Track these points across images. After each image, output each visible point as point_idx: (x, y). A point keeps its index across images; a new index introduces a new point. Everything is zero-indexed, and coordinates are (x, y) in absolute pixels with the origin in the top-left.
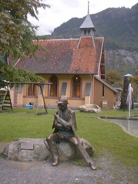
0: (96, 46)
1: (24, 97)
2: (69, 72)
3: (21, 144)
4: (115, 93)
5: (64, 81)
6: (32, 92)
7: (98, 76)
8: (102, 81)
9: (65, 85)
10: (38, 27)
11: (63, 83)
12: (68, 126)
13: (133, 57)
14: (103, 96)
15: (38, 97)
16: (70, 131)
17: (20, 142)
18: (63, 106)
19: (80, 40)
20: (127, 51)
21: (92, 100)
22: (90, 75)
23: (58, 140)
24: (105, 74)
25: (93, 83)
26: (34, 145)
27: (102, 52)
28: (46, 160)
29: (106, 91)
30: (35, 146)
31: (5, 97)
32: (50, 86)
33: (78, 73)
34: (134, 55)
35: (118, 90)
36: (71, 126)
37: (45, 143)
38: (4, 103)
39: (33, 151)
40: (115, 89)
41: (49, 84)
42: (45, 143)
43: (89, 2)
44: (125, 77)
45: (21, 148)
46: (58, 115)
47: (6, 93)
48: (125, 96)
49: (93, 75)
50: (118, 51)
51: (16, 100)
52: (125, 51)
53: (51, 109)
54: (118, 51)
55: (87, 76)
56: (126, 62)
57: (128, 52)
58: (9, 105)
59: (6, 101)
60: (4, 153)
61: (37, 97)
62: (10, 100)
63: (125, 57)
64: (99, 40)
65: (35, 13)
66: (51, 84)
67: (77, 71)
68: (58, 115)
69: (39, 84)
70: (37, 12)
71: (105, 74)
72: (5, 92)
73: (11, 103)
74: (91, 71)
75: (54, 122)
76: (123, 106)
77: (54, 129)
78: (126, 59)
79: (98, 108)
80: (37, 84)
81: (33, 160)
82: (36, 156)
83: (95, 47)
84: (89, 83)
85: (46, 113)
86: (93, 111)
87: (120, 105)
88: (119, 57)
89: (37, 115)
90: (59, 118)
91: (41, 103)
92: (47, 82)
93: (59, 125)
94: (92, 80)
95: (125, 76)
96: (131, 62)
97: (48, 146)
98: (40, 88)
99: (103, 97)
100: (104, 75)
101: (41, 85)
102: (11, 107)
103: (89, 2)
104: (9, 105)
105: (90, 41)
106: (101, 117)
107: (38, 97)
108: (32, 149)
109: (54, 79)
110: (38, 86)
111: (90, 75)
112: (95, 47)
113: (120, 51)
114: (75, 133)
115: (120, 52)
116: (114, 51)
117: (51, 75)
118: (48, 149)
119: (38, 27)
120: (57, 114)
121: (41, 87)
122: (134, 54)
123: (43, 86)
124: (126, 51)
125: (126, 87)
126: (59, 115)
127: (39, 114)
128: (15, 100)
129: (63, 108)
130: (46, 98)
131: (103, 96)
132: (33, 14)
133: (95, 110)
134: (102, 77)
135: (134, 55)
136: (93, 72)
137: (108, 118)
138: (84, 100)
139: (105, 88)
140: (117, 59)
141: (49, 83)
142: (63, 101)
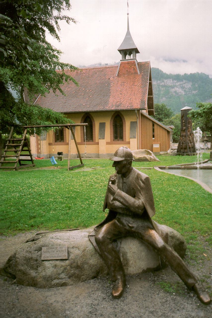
0: (141, 73)
1: (50, 144)
2: (107, 108)
3: (41, 249)
4: (168, 132)
5: (102, 121)
6: (60, 137)
7: (145, 112)
8: (150, 117)
9: (102, 126)
10: (61, 53)
11: (100, 123)
12: (139, 207)
13: (183, 88)
14: (154, 137)
15: (68, 143)
16: (143, 215)
17: (39, 245)
18: (124, 166)
19: (119, 67)
20: (174, 81)
21: (139, 142)
22: (135, 110)
23: (119, 235)
24: (153, 109)
25: (139, 122)
26: (68, 248)
27: (149, 81)
28: (94, 277)
29: (158, 131)
30: (71, 250)
31: (21, 147)
32: (85, 128)
33: (120, 108)
34: (184, 85)
35: (170, 128)
36: (144, 205)
37: (91, 242)
38: (21, 155)
39: (67, 262)
40: (167, 127)
41: (83, 126)
42: (91, 242)
43: (128, 14)
44: (181, 110)
45: (42, 259)
46: (116, 184)
47: (23, 141)
48: (183, 135)
49: (138, 111)
50: (163, 82)
51: (40, 149)
52: (172, 81)
53: (87, 157)
54: (163, 82)
55: (131, 112)
56: (174, 94)
57: (176, 81)
58: (29, 158)
59: (24, 153)
60: (8, 268)
61: (68, 144)
62: (29, 150)
63: (173, 87)
64: (144, 64)
65: (56, 29)
66: (86, 126)
67: (118, 106)
68: (116, 184)
69: (69, 126)
70: (59, 28)
71: (153, 109)
72: (21, 140)
73: (30, 155)
74: (136, 105)
75: (107, 198)
76: (182, 148)
77: (107, 210)
78: (173, 90)
79: (150, 154)
80: (66, 127)
81: (69, 281)
82: (75, 273)
83: (139, 73)
84: (134, 121)
85: (82, 165)
86: (144, 158)
87: (177, 148)
88: (164, 88)
89: (68, 170)
90: (119, 190)
91: (73, 151)
92: (78, 122)
93: (117, 204)
94: (138, 117)
95: (181, 109)
96: (179, 93)
97: (97, 248)
98: (70, 131)
99: (153, 139)
100: (152, 110)
101: (72, 127)
102: (32, 160)
103: (128, 14)
104: (29, 158)
105: (133, 67)
106: (161, 168)
107: (69, 143)
108: (65, 258)
109: (88, 117)
110: (68, 129)
111: (135, 110)
112: (139, 73)
113: (165, 81)
114: (153, 218)
115: (166, 82)
116: (159, 82)
117: (83, 115)
118: (99, 253)
119: (61, 53)
120: (113, 182)
121: (72, 131)
122: (183, 84)
123: (74, 129)
124: (173, 81)
125: (184, 124)
126: (118, 185)
127: (71, 169)
128: (38, 149)
129: (124, 170)
130: (80, 144)
131: (154, 137)
132: (52, 30)
133: (148, 157)
134: (150, 113)
135: (184, 85)
136: (139, 107)
137: (170, 168)
138: (129, 144)
139: (155, 126)
140: (163, 91)
141: (83, 124)
142: (123, 157)
